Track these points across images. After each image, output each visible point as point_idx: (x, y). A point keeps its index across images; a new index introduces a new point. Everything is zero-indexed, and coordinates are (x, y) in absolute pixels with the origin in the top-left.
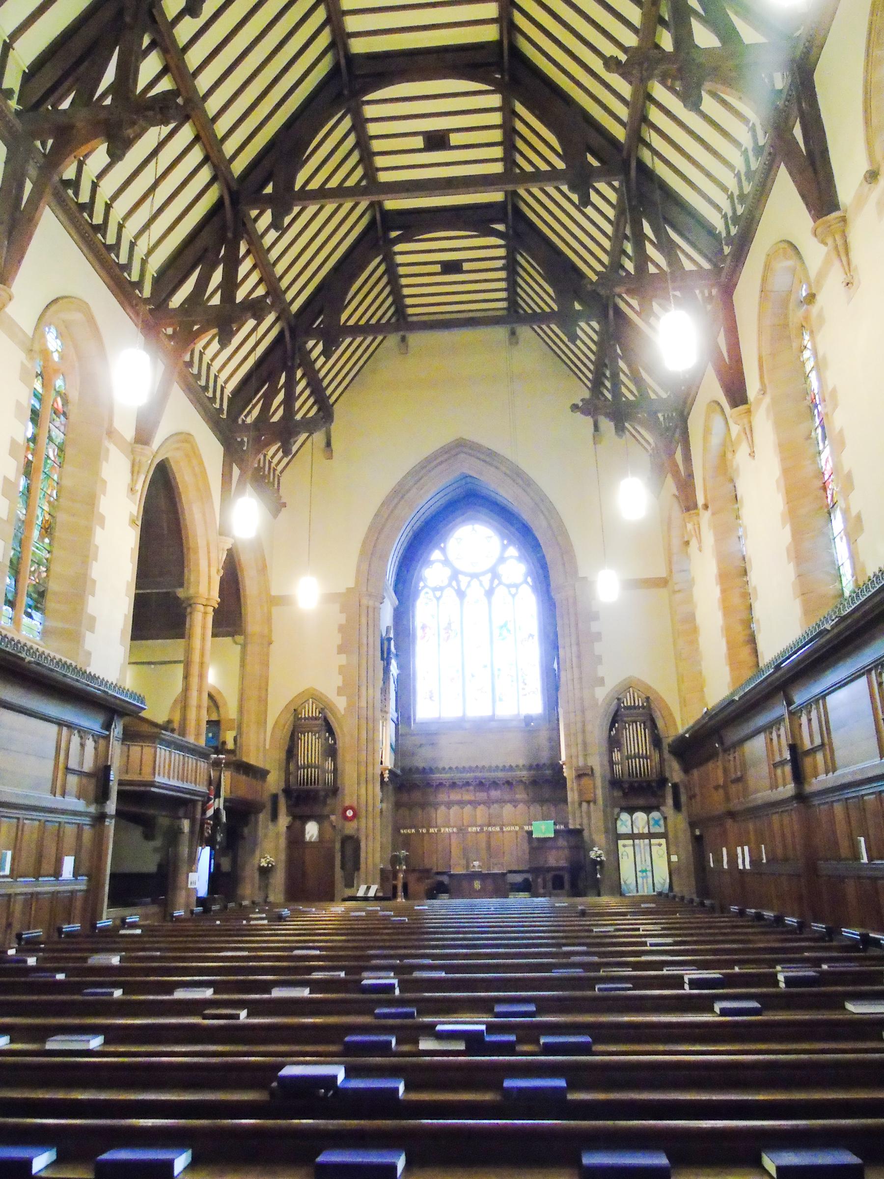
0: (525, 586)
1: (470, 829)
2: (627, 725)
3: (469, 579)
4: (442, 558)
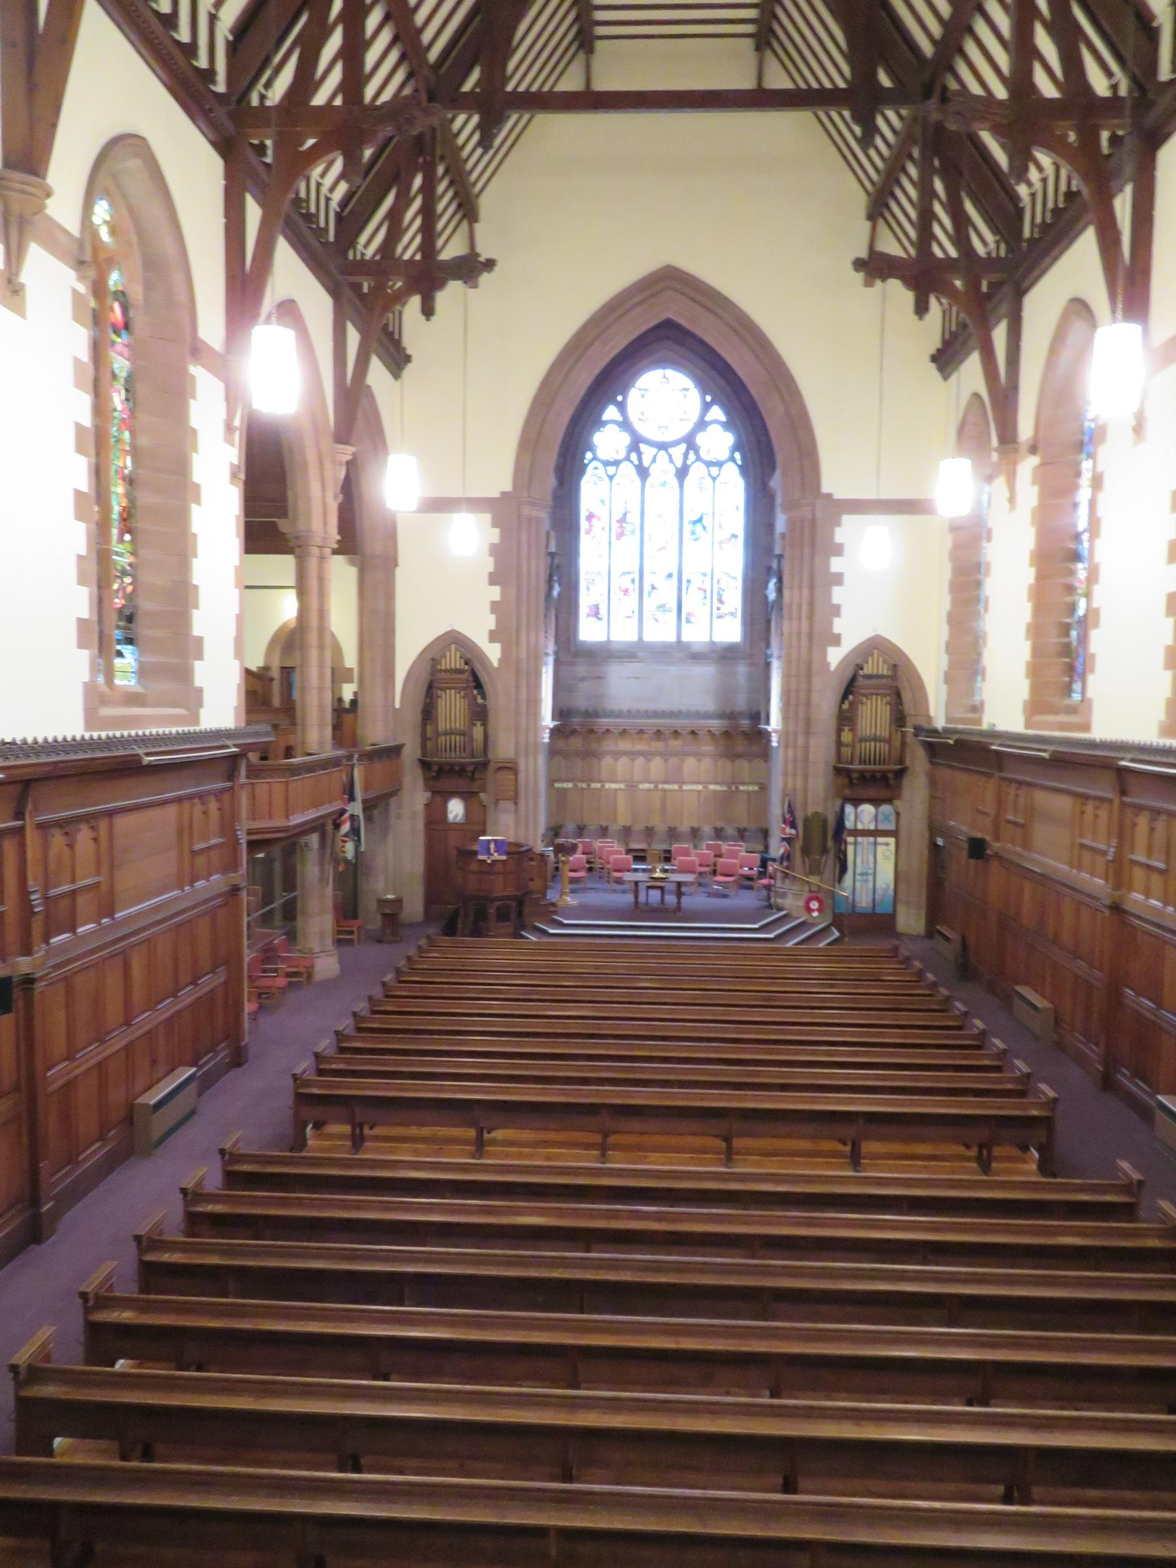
0: (731, 464)
1: (641, 786)
3: (654, 450)
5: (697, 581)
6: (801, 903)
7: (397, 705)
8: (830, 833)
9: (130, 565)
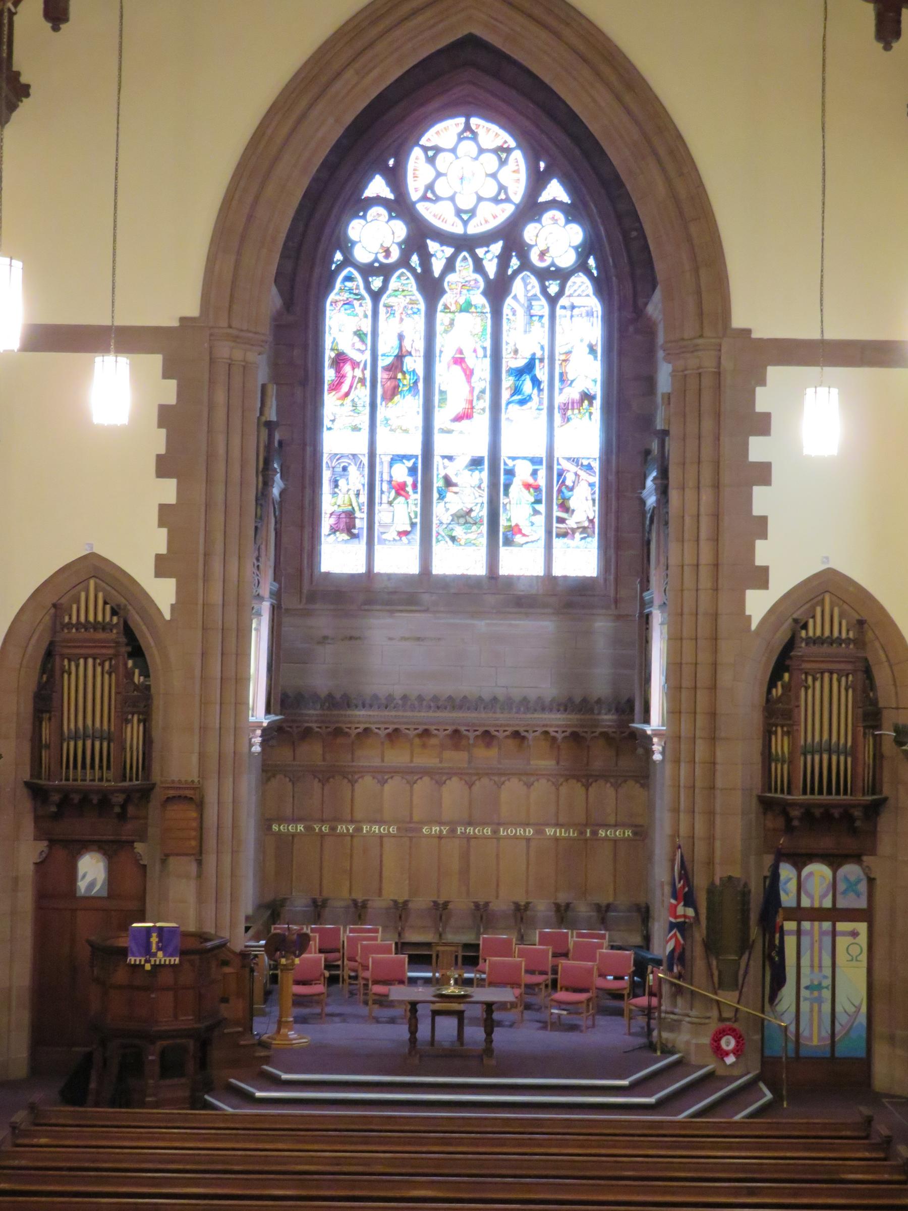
2: (810, 679)
4: (387, 193)
5: (523, 471)
6: (706, 1040)
8: (754, 917)
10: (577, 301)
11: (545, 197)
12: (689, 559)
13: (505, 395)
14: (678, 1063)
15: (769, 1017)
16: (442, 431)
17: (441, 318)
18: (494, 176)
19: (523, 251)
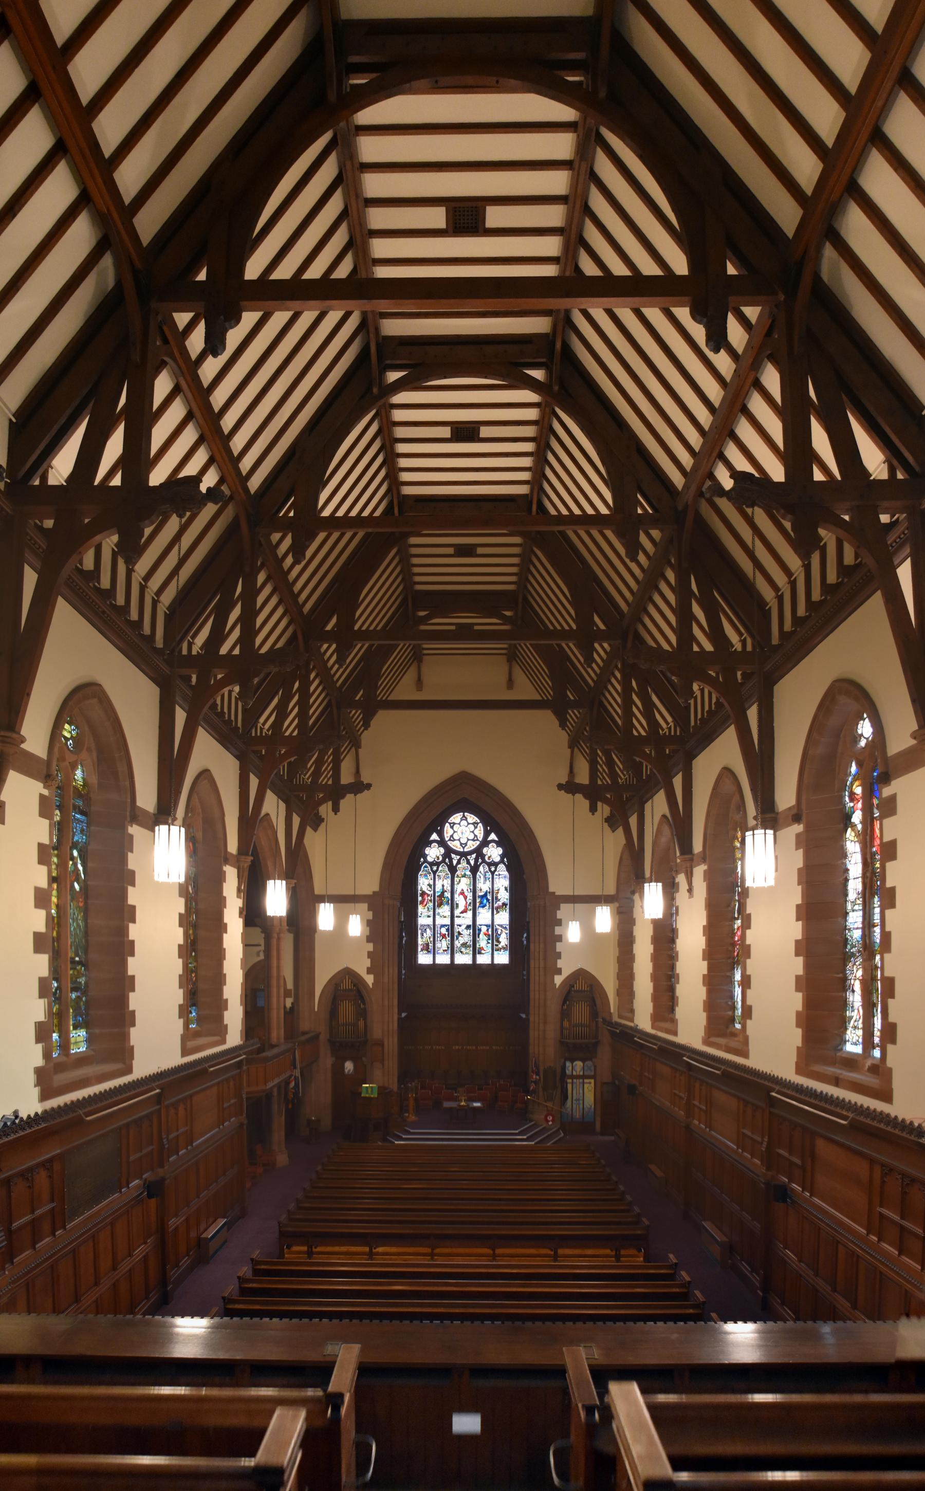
4: (438, 838)
5: (484, 929)
6: (543, 1117)
7: (316, 1009)
8: (558, 1078)
9: (194, 967)
10: (501, 873)
11: (490, 839)
12: (537, 966)
13: (478, 904)
14: (535, 1124)
15: (563, 1110)
16: (457, 917)
17: (456, 879)
18: (473, 832)
19: (483, 856)
